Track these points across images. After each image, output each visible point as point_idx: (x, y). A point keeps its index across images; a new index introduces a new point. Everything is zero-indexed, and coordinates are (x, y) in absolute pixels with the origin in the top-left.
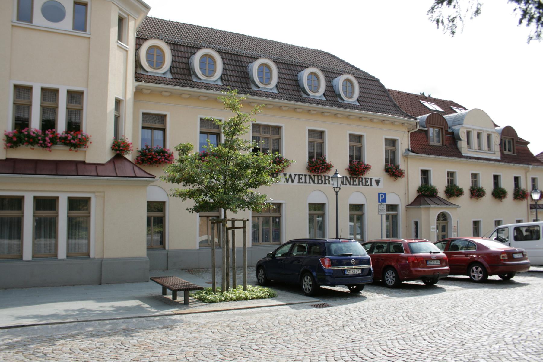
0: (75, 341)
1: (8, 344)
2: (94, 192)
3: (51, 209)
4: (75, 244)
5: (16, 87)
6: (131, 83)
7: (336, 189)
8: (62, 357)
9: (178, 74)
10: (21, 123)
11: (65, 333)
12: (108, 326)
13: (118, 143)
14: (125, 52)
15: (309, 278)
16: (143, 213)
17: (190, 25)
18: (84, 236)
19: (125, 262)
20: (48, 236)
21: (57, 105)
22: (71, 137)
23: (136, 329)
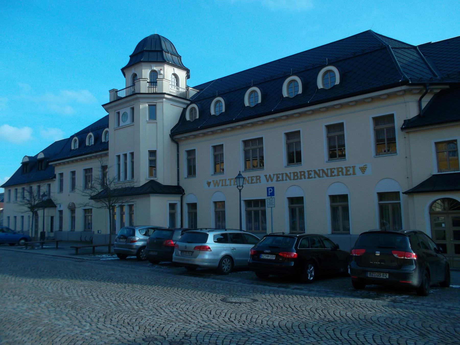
7: (239, 187)
15: (229, 260)
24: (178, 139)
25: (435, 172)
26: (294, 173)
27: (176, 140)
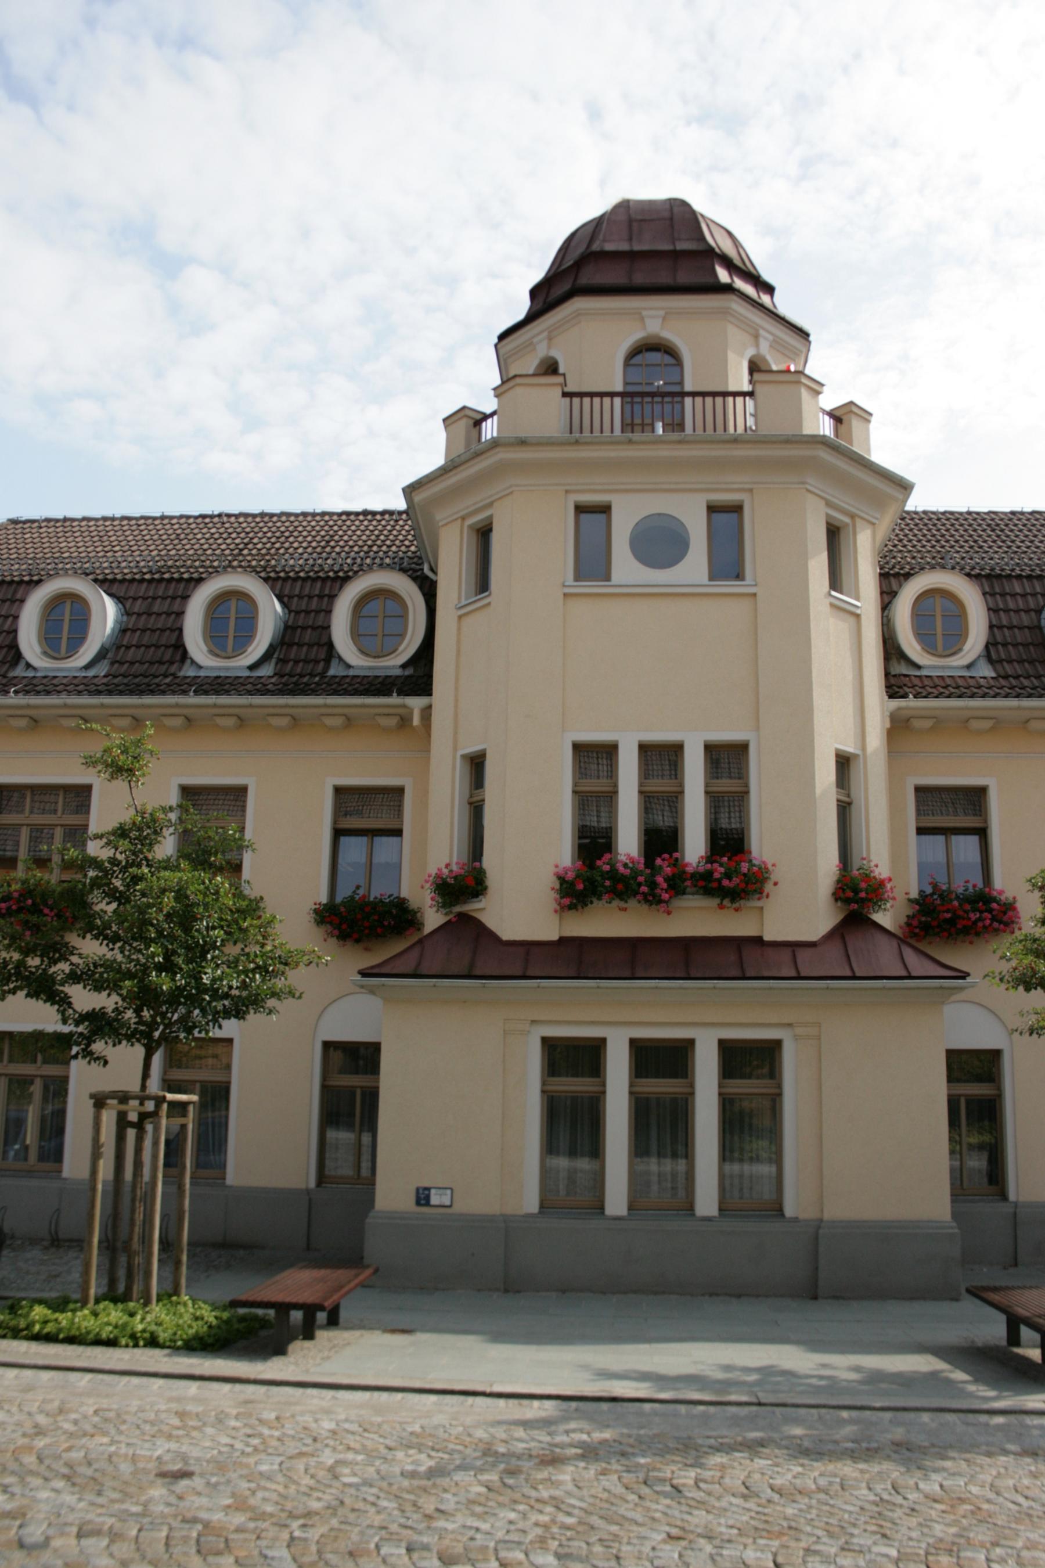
0: (756, 1460)
1: (581, 1445)
2: (790, 1025)
3: (675, 1075)
4: (741, 1176)
5: (579, 748)
6: (877, 706)
8: (723, 1503)
9: (1010, 662)
10: (593, 842)
11: (725, 1432)
12: (848, 1430)
13: (852, 879)
14: (852, 620)
16: (935, 1089)
17: (1032, 513)
18: (764, 1155)
19: (887, 1235)
20: (654, 1148)
21: (682, 785)
22: (722, 870)
23: (933, 1445)
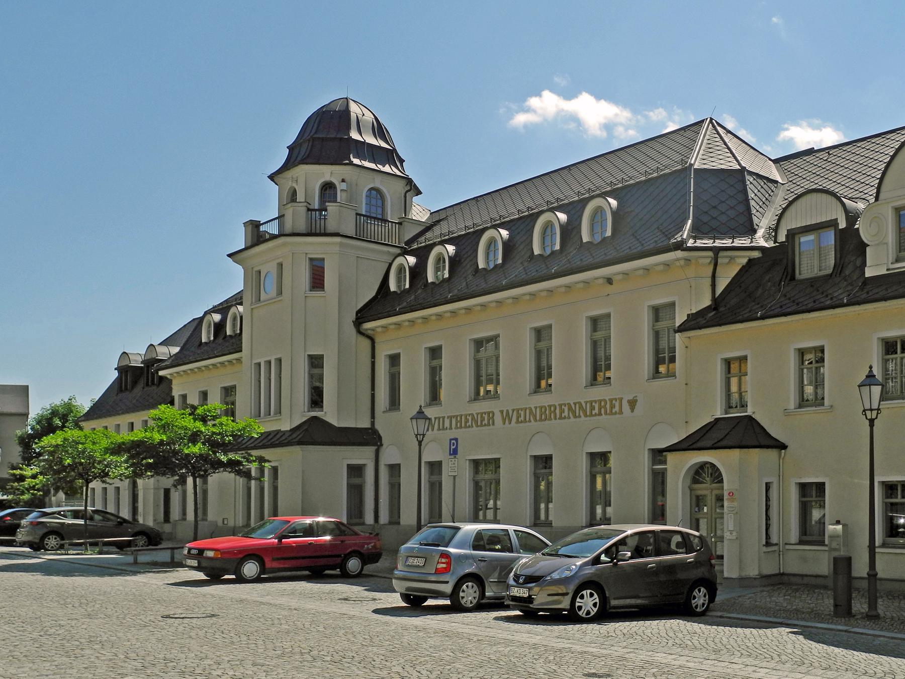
7: (868, 413)
15: (702, 589)
24: (373, 330)
25: (719, 414)
26: (541, 408)
27: (370, 332)
